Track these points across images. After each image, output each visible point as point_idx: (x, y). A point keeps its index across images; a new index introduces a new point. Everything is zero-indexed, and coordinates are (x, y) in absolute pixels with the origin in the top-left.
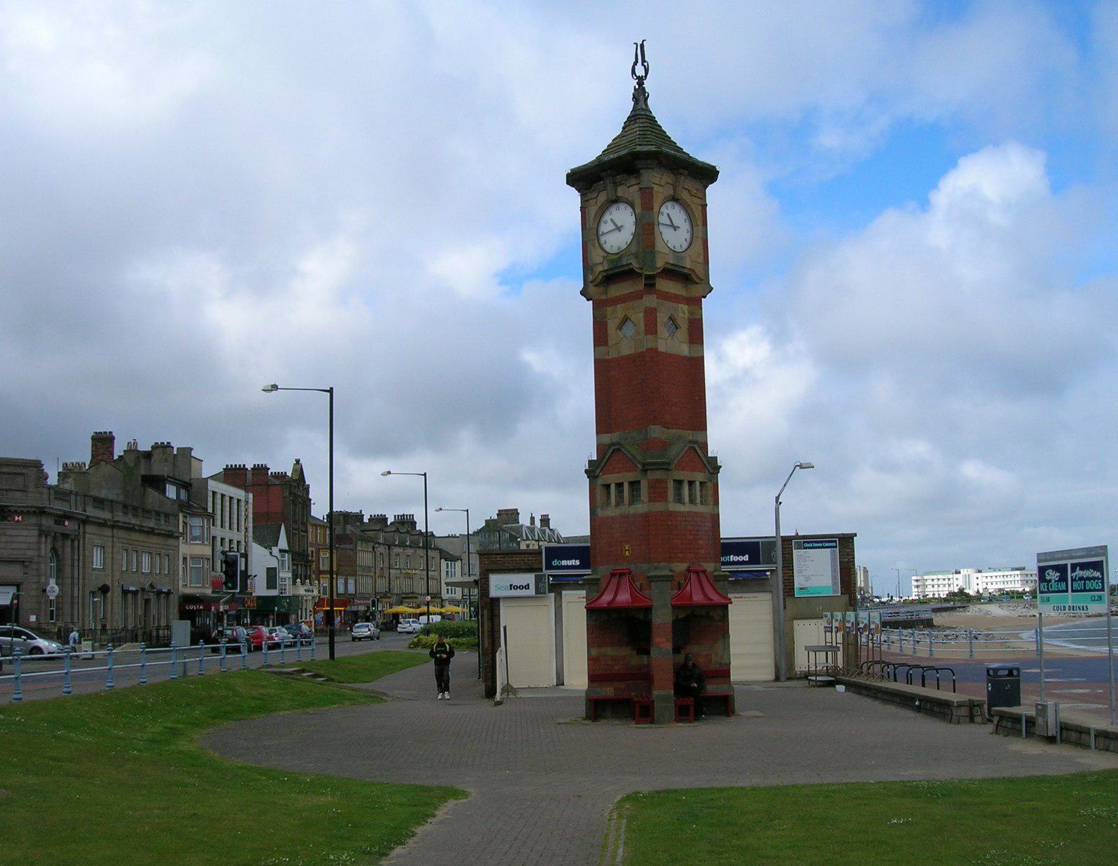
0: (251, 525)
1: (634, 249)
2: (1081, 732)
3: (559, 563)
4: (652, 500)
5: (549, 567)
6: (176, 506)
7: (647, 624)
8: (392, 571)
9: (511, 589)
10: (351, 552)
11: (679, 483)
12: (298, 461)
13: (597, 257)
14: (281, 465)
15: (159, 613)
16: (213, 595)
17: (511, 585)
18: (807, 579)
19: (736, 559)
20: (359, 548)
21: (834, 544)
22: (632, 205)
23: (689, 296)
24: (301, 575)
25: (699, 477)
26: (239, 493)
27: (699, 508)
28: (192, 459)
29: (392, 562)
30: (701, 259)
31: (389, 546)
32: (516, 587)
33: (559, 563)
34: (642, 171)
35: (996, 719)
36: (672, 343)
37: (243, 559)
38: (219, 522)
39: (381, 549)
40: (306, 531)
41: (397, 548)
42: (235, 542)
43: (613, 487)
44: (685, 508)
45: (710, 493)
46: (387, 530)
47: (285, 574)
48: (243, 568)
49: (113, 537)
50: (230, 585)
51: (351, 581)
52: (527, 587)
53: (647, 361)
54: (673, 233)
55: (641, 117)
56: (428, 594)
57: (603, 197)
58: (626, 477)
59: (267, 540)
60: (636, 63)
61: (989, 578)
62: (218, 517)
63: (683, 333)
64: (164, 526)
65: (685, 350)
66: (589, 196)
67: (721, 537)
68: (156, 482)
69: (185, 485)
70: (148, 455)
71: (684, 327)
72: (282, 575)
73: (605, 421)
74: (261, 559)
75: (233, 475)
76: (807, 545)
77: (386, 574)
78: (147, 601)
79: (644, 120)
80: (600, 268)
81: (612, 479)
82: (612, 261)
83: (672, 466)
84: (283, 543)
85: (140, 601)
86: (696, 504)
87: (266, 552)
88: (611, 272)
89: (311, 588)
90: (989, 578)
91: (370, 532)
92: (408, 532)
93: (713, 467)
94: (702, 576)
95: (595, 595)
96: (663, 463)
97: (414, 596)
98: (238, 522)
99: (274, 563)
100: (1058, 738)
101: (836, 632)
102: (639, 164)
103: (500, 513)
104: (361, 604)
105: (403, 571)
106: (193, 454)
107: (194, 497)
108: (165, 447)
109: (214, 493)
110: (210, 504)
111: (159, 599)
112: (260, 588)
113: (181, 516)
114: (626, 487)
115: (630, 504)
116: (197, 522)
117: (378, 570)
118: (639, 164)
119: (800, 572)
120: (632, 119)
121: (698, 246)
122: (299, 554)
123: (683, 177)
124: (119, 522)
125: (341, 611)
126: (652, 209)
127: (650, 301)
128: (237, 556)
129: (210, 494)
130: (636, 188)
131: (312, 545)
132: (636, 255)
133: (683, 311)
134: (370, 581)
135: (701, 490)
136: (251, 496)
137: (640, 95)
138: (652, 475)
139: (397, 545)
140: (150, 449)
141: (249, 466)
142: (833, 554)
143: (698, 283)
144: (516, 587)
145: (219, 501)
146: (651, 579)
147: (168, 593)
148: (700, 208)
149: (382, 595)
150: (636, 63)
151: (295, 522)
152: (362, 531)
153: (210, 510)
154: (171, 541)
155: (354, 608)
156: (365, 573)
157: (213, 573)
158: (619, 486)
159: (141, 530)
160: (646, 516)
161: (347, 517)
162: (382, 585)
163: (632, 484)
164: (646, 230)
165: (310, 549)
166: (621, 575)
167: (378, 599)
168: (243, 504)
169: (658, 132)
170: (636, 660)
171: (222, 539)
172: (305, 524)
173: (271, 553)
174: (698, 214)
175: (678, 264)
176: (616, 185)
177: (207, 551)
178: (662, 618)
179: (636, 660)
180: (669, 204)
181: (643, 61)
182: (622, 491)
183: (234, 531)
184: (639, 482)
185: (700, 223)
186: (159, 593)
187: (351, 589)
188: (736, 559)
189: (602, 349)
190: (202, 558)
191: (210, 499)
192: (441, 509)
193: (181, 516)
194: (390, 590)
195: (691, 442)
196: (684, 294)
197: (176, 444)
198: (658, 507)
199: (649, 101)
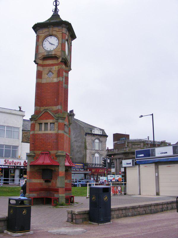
5: (137, 157)
13: (41, 51)
44: (43, 132)
52: (130, 164)
55: (56, 14)
73: (36, 104)
88: (47, 56)
137: (56, 10)
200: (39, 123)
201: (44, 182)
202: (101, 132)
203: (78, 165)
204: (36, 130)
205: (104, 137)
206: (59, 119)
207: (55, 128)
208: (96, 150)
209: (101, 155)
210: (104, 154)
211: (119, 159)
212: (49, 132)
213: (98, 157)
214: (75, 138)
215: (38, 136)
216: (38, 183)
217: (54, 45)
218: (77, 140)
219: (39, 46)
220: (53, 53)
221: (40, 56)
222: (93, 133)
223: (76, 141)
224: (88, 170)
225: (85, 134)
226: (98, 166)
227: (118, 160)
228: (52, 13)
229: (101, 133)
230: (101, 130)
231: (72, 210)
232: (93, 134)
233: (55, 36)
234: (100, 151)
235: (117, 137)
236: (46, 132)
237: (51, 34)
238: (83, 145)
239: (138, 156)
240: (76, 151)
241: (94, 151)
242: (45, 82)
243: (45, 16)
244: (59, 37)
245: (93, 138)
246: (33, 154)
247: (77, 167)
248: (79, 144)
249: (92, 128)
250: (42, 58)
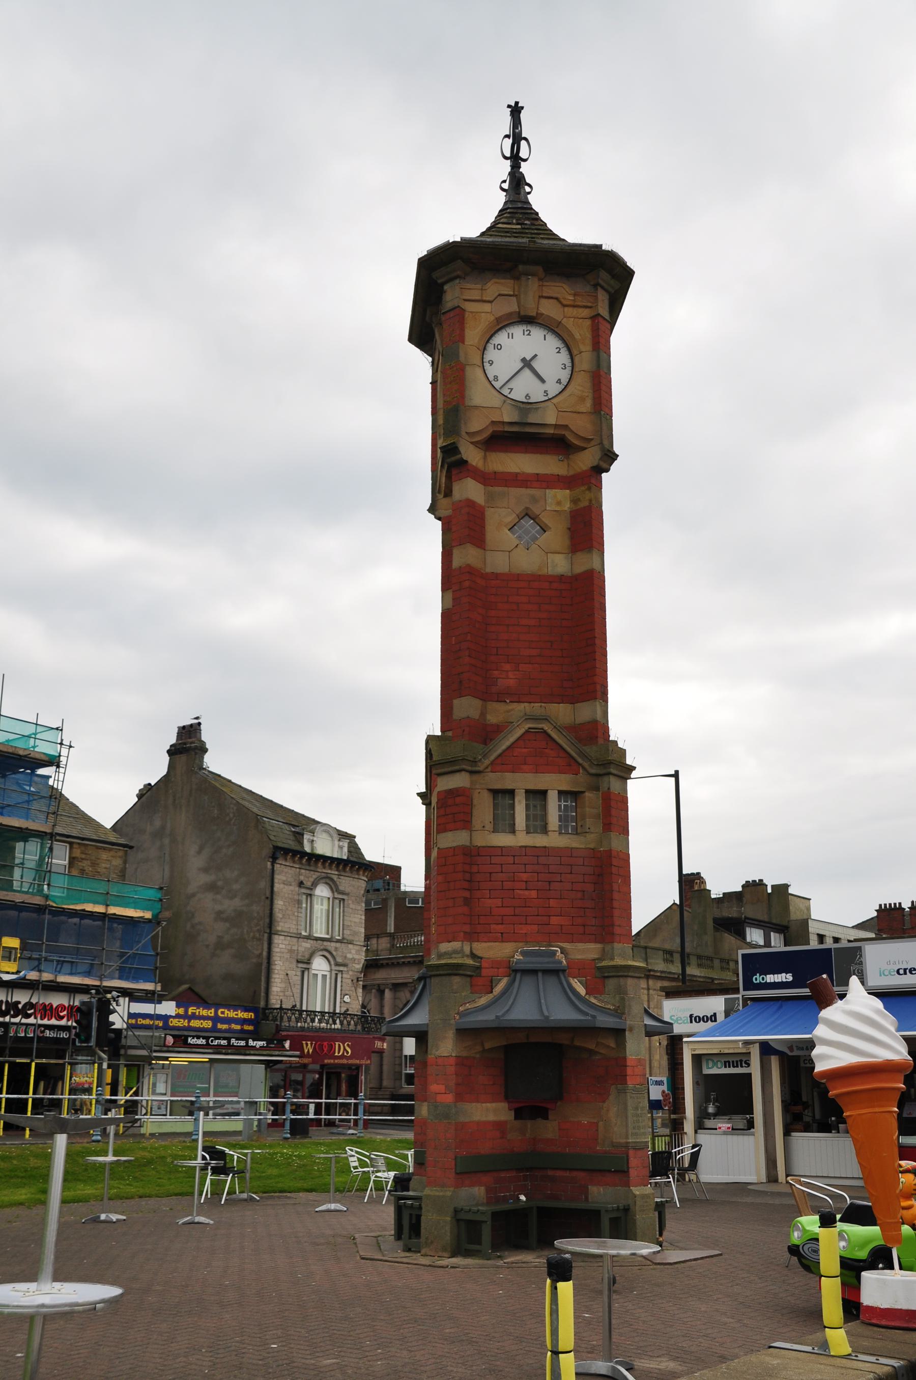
3: (763, 979)
9: (691, 1022)
17: (691, 1016)
23: (571, 473)
33: (763, 979)
49: (648, 989)
63: (556, 536)
65: (560, 565)
124: (654, 971)
133: (557, 501)
137: (517, 184)
140: (740, 889)
141: (906, 905)
143: (586, 448)
197: (770, 882)
200: (490, 790)
201: (510, 1116)
202: (345, 844)
203: (231, 1014)
204: (476, 823)
205: (358, 870)
206: (609, 774)
207: (589, 822)
208: (317, 939)
209: (338, 965)
210: (353, 960)
211: (396, 987)
212: (554, 840)
213: (324, 976)
214: (206, 870)
215: (495, 860)
216: (489, 1123)
218: (220, 883)
219: (468, 369)
220: (551, 417)
221: (477, 424)
222: (307, 849)
223: (212, 887)
224: (287, 1045)
225: (267, 851)
226: (313, 1021)
227: (388, 994)
228: (499, 200)
229: (346, 850)
230: (343, 835)
232: (306, 854)
233: (553, 327)
234: (338, 945)
235: (773, 886)
236: (539, 840)
237: (534, 314)
238: (257, 909)
239: (758, 979)
240: (212, 939)
241: (307, 945)
242: (506, 570)
243: (471, 214)
244: (577, 336)
245: (308, 876)
246: (470, 962)
247: (225, 1027)
248: (230, 905)
249: (300, 824)
250: (486, 435)
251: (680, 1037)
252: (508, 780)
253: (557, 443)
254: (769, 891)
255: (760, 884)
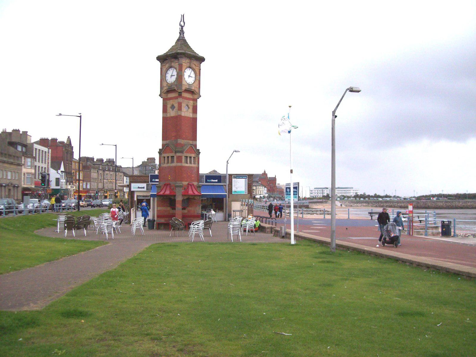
0: (50, 161)
1: (176, 83)
2: (344, 248)
4: (177, 162)
5: (151, 181)
6: (21, 154)
7: (174, 201)
8: (104, 180)
10: (89, 173)
11: (187, 157)
12: (69, 137)
13: (165, 84)
14: (62, 138)
15: (14, 194)
16: (35, 188)
17: (138, 187)
18: (237, 188)
19: (214, 181)
20: (92, 171)
21: (246, 177)
22: (176, 69)
24: (69, 181)
25: (193, 155)
26: (46, 149)
27: (193, 165)
28: (28, 136)
29: (105, 177)
30: (198, 87)
31: (104, 171)
32: (140, 188)
34: (179, 59)
35: (273, 233)
36: (186, 113)
37: (48, 176)
38: (38, 160)
39: (101, 172)
40: (71, 164)
41: (107, 171)
42: (44, 168)
43: (166, 158)
45: (197, 160)
46: (103, 164)
47: (63, 181)
48: (48, 179)
50: (43, 184)
51: (89, 184)
52: (144, 188)
53: (178, 119)
54: (189, 77)
56: (116, 190)
57: (167, 66)
58: (170, 155)
59: (56, 167)
60: (181, 21)
61: (341, 191)
62: (37, 158)
63: (191, 110)
64: (16, 162)
65: (191, 115)
66: (163, 65)
67: (200, 173)
68: (13, 144)
69: (24, 146)
70: (10, 134)
71: (191, 108)
72: (62, 181)
73: (164, 138)
74: (54, 174)
75: (43, 142)
76: (237, 177)
77: (102, 181)
78: (10, 190)
79: (182, 41)
80: (165, 88)
81: (166, 155)
82: (169, 86)
83: (184, 152)
84: (62, 169)
85: (7, 190)
86: (191, 164)
87: (55, 172)
89: (73, 186)
90: (341, 191)
91: (96, 165)
92: (111, 165)
93: (198, 152)
94: (192, 186)
95: (159, 191)
96: (182, 151)
97: (113, 190)
98: (42, 155)
99: (58, 176)
100: (285, 236)
101: (246, 206)
102: (179, 56)
103: (148, 159)
104: (92, 193)
105: (109, 181)
106: (28, 134)
107: (28, 150)
108: (16, 131)
109: (36, 149)
110: (34, 153)
111: (14, 190)
112: (53, 186)
113: (23, 158)
114: (170, 158)
115: (171, 163)
116: (29, 160)
117: (99, 179)
118: (179, 56)
119: (234, 186)
120: (178, 40)
121: (197, 82)
122: (69, 173)
123: (193, 61)
125: (84, 195)
126: (182, 71)
127: (180, 100)
128: (45, 175)
129: (34, 149)
130: (177, 64)
131: (74, 169)
132: (176, 85)
133: (191, 103)
134: (96, 184)
135: (194, 160)
136: (50, 150)
137: (182, 32)
138: (178, 154)
139: (107, 170)
141: (50, 139)
142: (245, 181)
143: (196, 94)
144: (140, 188)
145: (41, 153)
146: (176, 187)
147: (18, 187)
148: (198, 70)
149: (100, 190)
150: (181, 21)
151: (67, 160)
152: (94, 165)
153: (34, 155)
154: (19, 167)
155: (89, 194)
156: (94, 181)
157: (35, 180)
158: (168, 157)
159: (8, 163)
160: (175, 167)
161: (88, 159)
162: (100, 186)
163: (172, 157)
164: (180, 77)
165: (73, 171)
166: (167, 185)
167: (98, 191)
168: (47, 153)
169: (186, 45)
170: (172, 211)
171: (42, 167)
172: (71, 162)
173: (57, 172)
174: (198, 72)
175: (190, 88)
176: (172, 62)
177: (33, 171)
178: (179, 198)
179: (172, 211)
180: (188, 69)
181: (183, 21)
182: (169, 159)
183: (44, 164)
184: (174, 156)
185: (198, 75)
186: (14, 187)
187: (88, 187)
188: (214, 181)
189: (164, 114)
190: (31, 173)
191: (34, 151)
192: (123, 158)
193: (23, 158)
194: (104, 188)
195: (191, 144)
196: (192, 98)
198: (179, 164)
199: (185, 34)
217: (192, 77)
228: (177, 36)
231: (444, 220)
239: (153, 180)
243: (166, 45)
251: (133, 192)
252: (189, 155)
253: (192, 92)
254: (21, 133)
255: (19, 131)
